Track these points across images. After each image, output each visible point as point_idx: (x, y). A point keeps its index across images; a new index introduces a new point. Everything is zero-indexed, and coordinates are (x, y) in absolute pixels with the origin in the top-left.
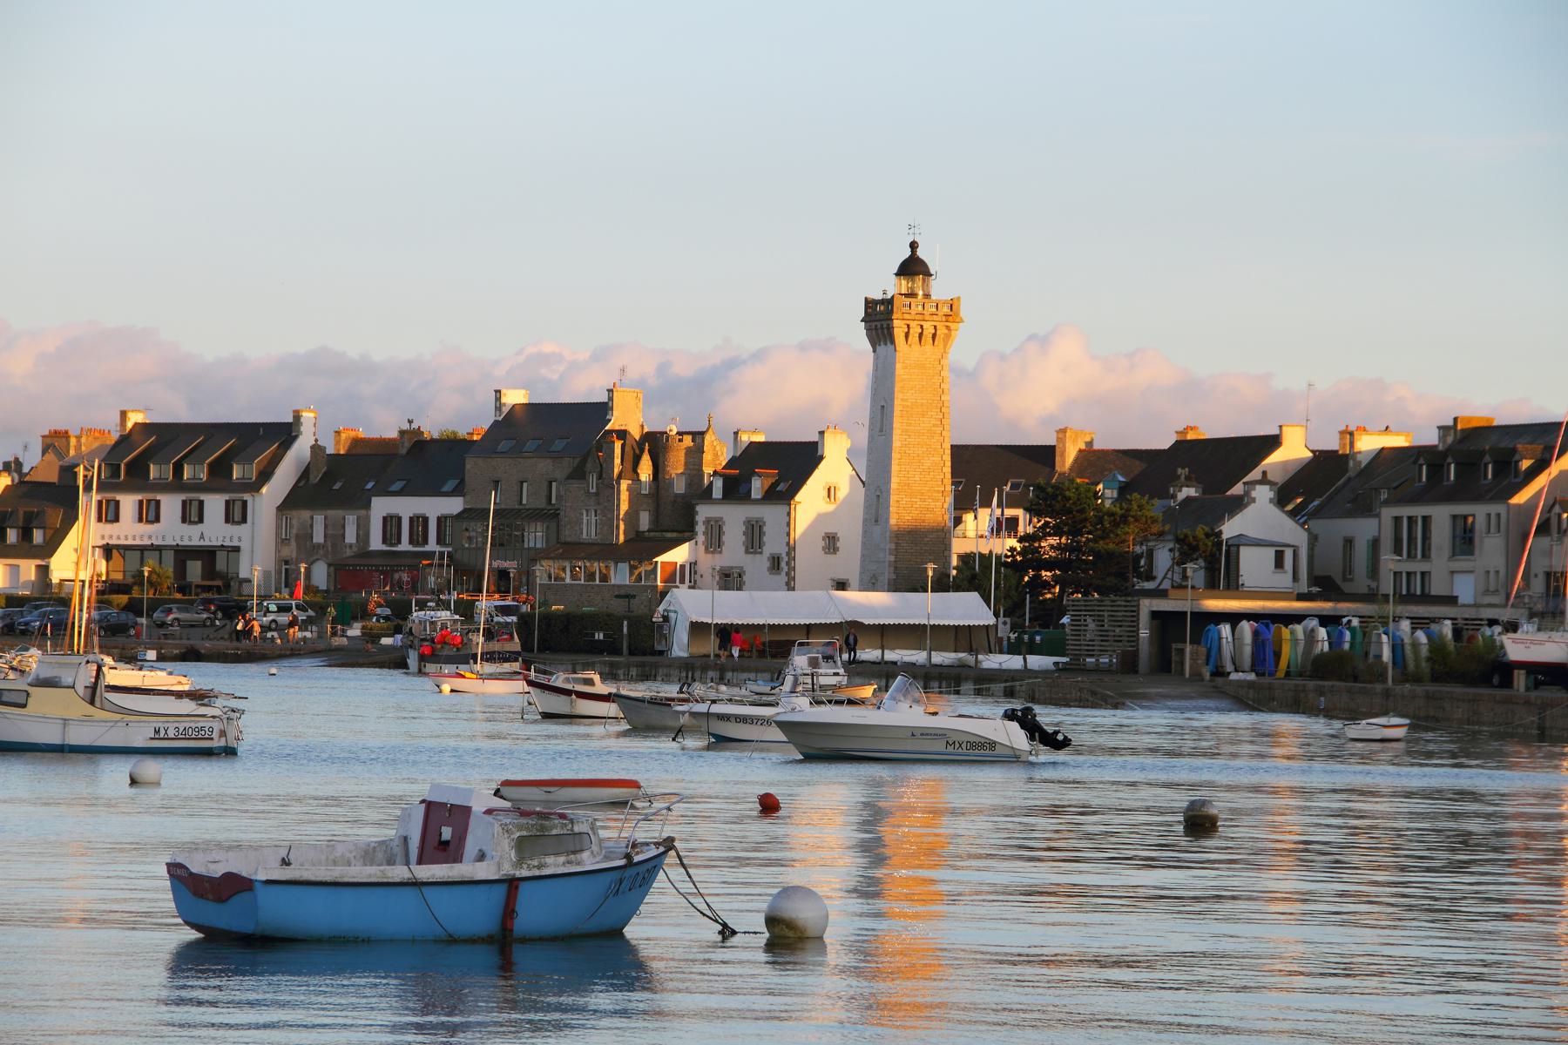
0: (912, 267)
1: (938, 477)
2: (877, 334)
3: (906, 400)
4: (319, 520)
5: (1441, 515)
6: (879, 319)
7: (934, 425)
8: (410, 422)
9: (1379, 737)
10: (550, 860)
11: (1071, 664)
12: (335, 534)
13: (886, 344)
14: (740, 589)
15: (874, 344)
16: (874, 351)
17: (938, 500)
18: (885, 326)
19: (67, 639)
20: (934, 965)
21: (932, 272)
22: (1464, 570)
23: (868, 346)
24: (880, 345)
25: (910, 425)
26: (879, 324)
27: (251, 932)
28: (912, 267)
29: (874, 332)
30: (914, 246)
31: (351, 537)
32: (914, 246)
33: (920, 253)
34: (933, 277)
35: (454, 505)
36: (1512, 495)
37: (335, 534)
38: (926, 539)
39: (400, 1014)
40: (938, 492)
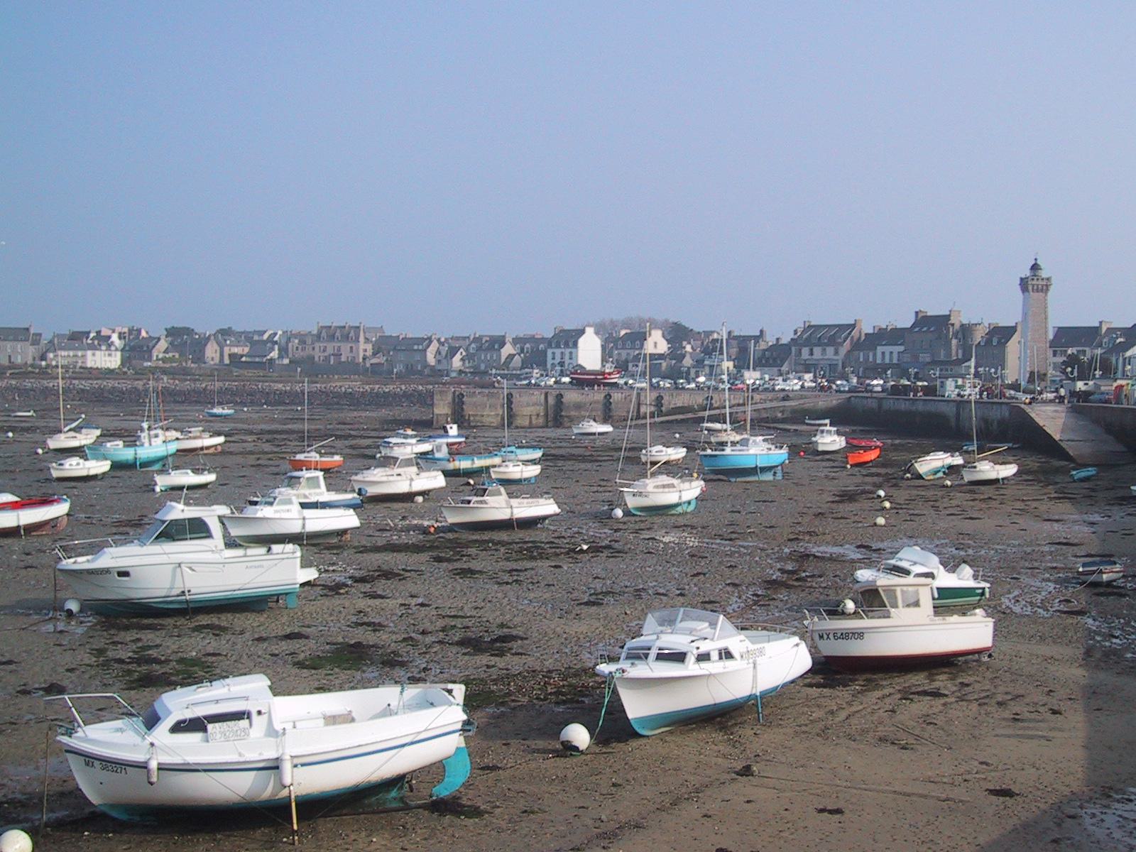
0: (1035, 267)
4: (862, 354)
6: (1024, 284)
10: (80, 559)
11: (910, 450)
12: (866, 359)
15: (1023, 292)
19: (756, 357)
20: (725, 481)
23: (1020, 292)
27: (748, 694)
28: (1035, 267)
30: (1036, 259)
31: (871, 360)
32: (1036, 259)
33: (1038, 262)
35: (901, 348)
36: (1127, 350)
37: (866, 359)
39: (769, 428)
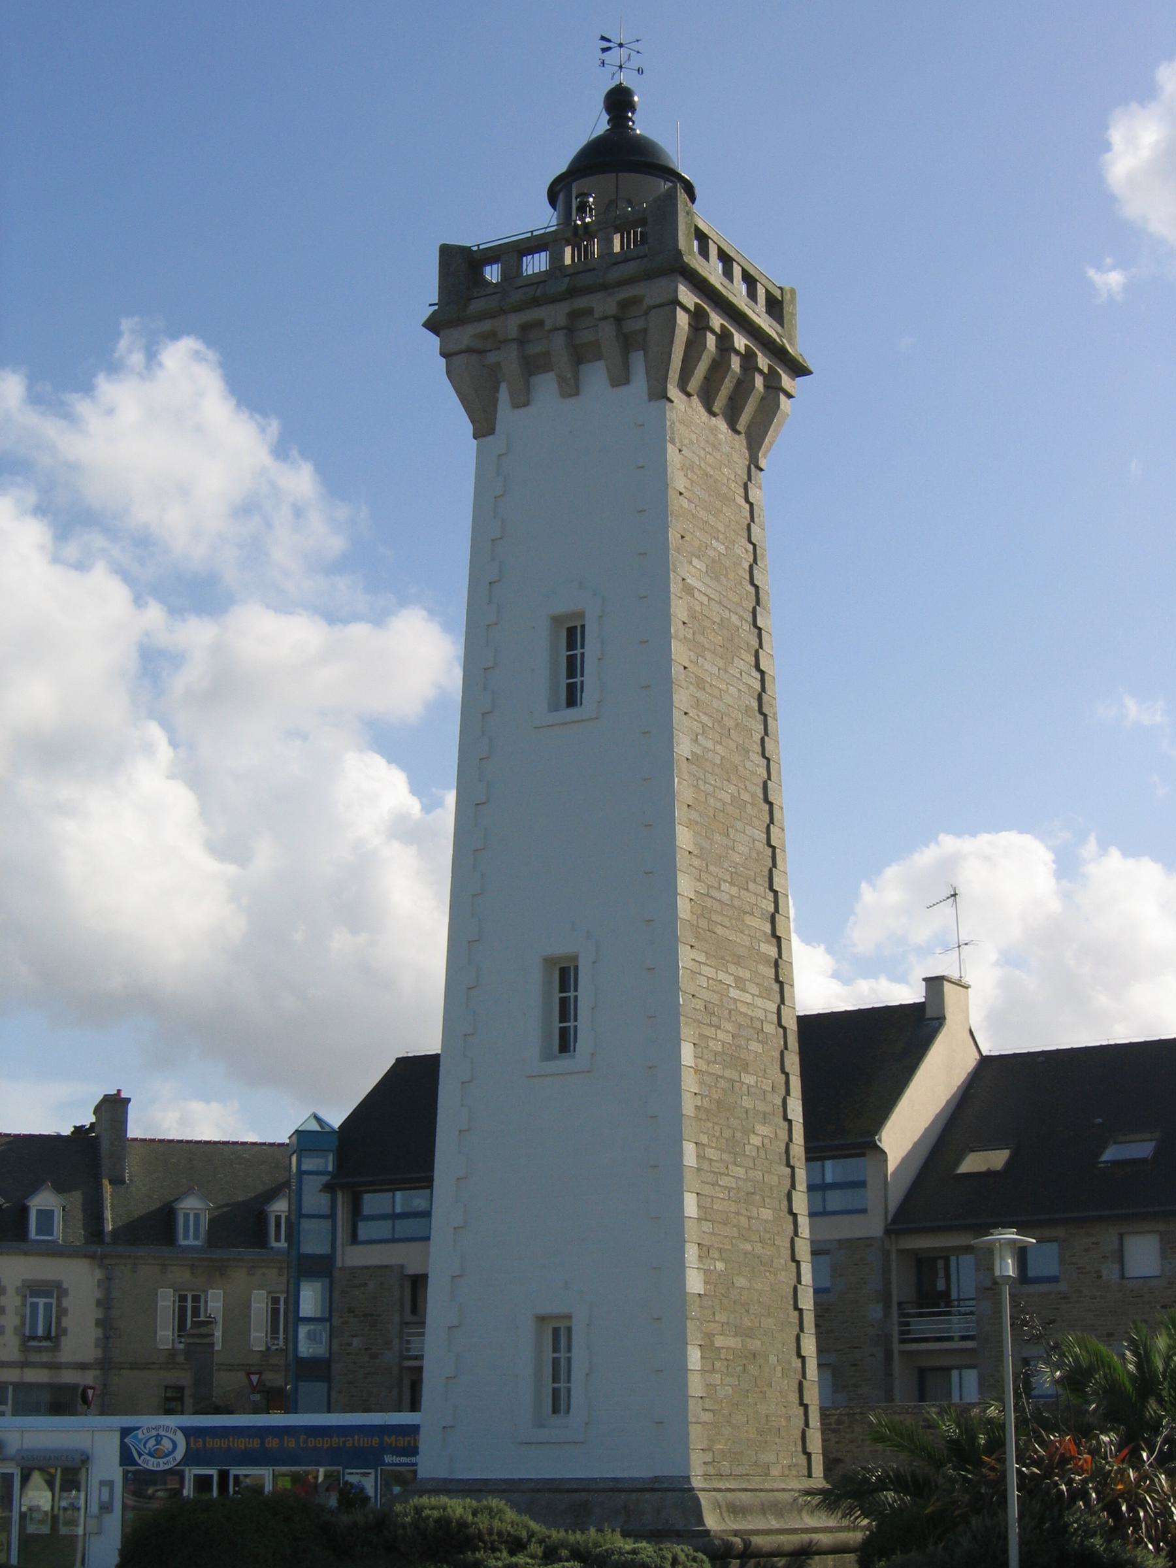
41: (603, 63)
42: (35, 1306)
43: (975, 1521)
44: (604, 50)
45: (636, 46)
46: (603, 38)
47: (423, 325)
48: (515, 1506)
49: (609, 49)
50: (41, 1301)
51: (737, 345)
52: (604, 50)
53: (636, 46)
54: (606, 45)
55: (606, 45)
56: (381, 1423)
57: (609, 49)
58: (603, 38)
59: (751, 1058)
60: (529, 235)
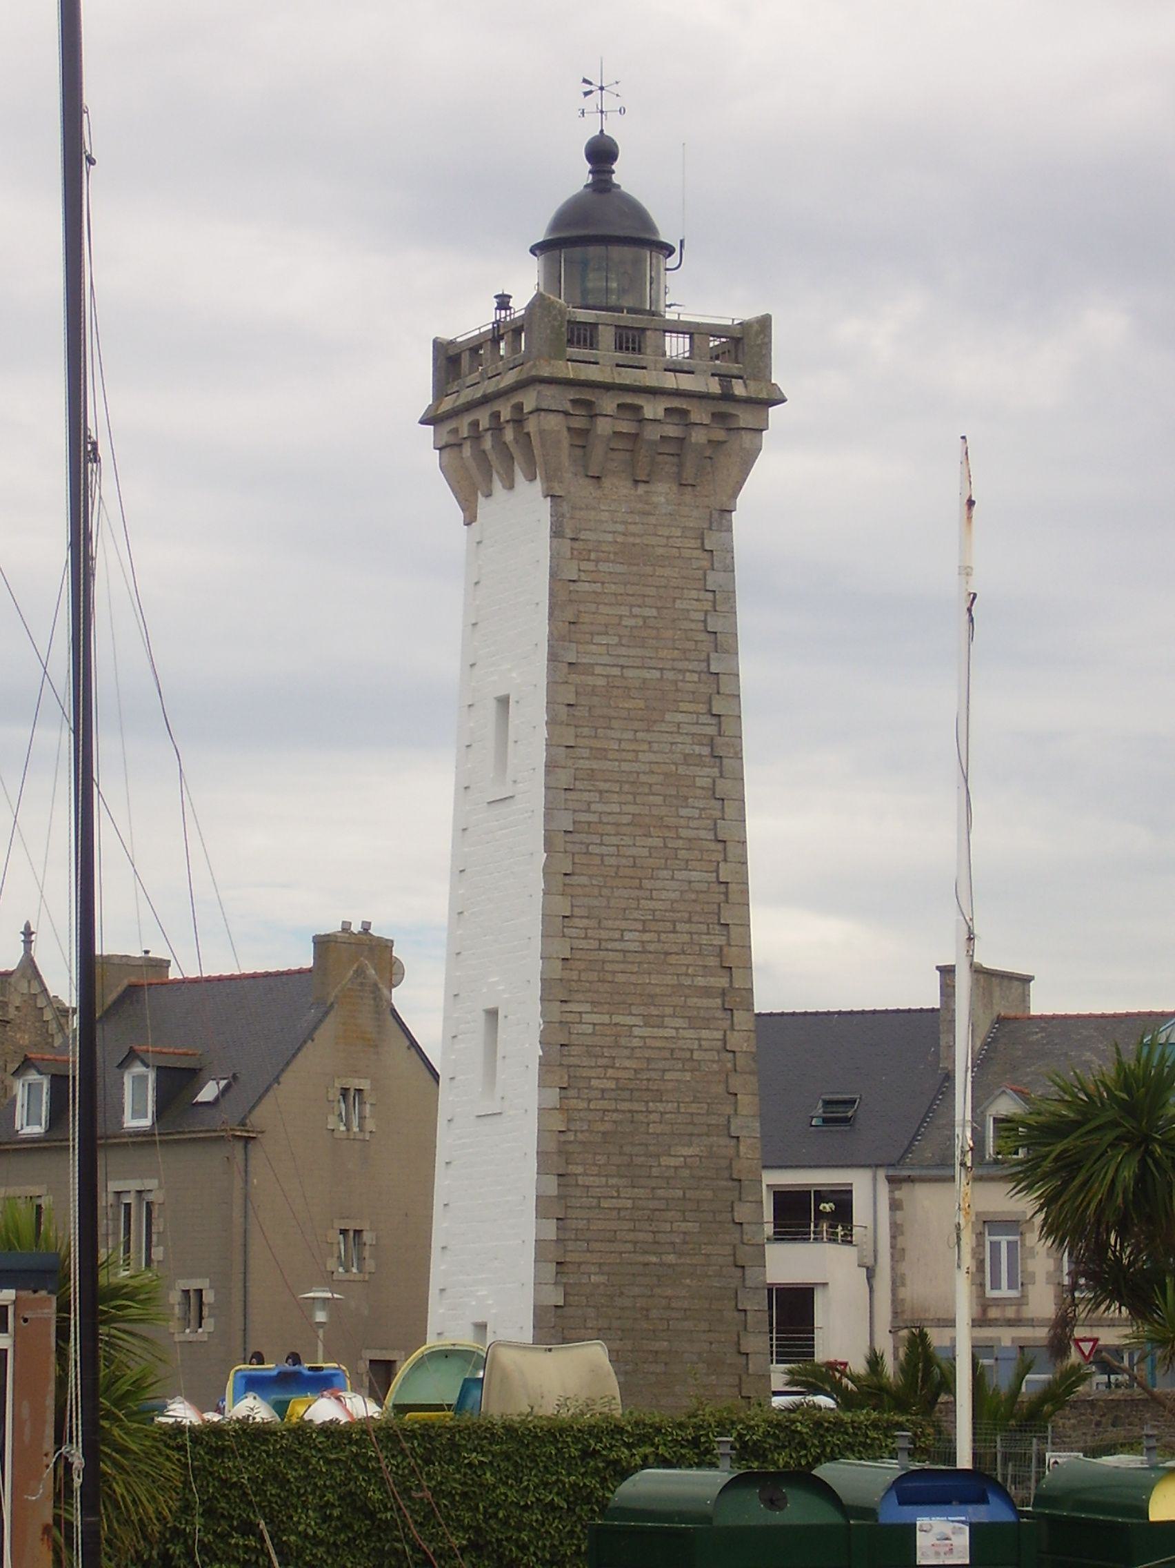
1: (705, 939)
2: (481, 456)
3: (588, 669)
5: (359, 1492)
7: (687, 759)
8: (481, 1327)
9: (242, 1318)
13: (510, 486)
14: (851, 1191)
16: (470, 520)
17: (707, 1023)
18: (506, 414)
21: (666, 235)
22: (871, 1201)
24: (488, 495)
25: (601, 754)
26: (483, 417)
29: (467, 450)
34: (672, 261)
38: (665, 1161)
40: (706, 992)
41: (583, 113)
42: (995, 1246)
43: (205, 1498)
44: (586, 94)
45: (615, 89)
46: (585, 81)
47: (435, 342)
48: (190, 1436)
49: (591, 92)
50: (1004, 1240)
51: (61, 1040)
52: (586, 94)
53: (615, 89)
54: (588, 88)
55: (588, 88)
56: (128, 1182)
57: (591, 92)
58: (585, 81)
59: (522, 1536)
60: (477, 332)
